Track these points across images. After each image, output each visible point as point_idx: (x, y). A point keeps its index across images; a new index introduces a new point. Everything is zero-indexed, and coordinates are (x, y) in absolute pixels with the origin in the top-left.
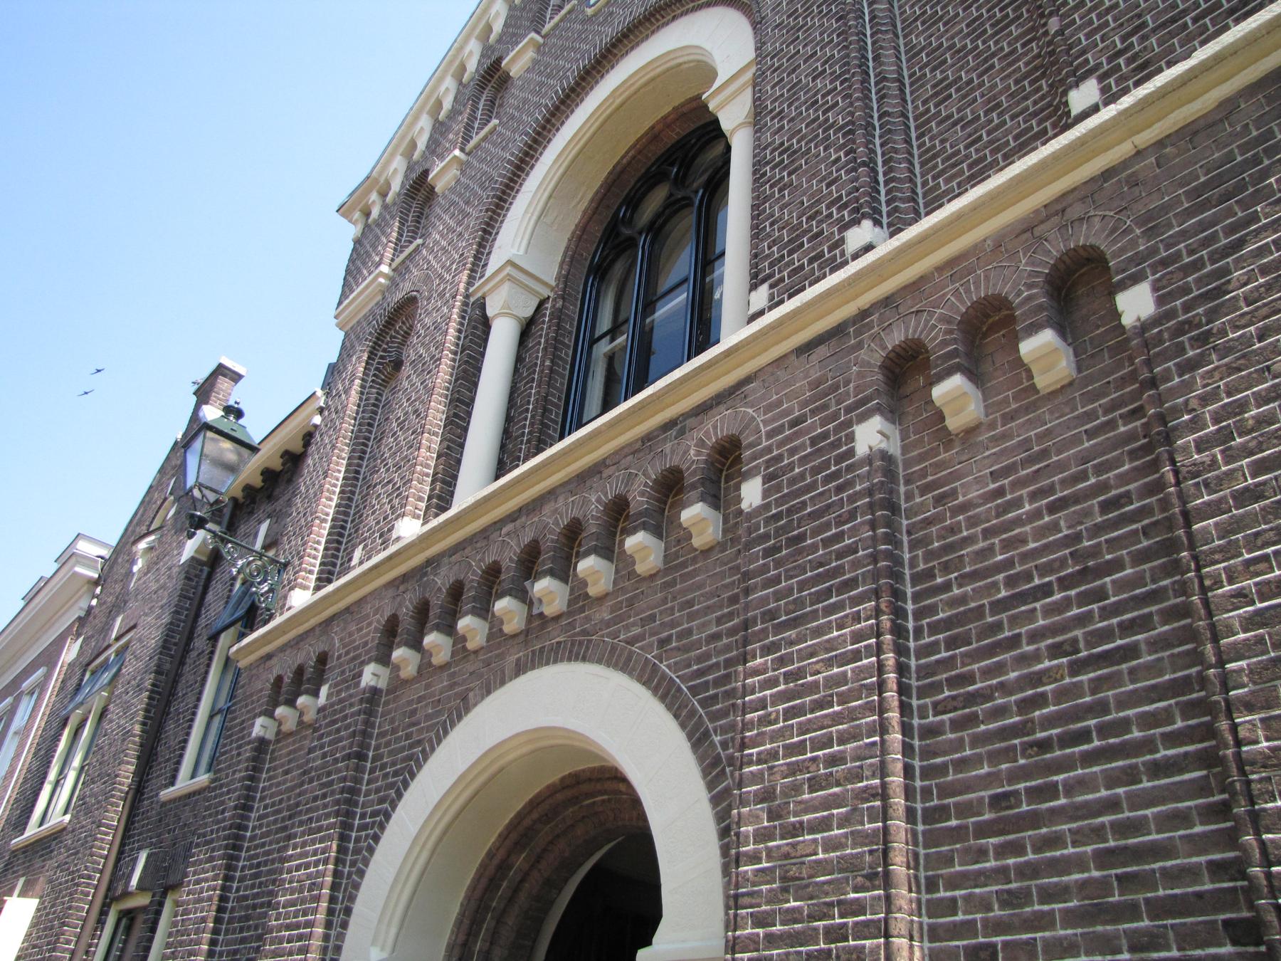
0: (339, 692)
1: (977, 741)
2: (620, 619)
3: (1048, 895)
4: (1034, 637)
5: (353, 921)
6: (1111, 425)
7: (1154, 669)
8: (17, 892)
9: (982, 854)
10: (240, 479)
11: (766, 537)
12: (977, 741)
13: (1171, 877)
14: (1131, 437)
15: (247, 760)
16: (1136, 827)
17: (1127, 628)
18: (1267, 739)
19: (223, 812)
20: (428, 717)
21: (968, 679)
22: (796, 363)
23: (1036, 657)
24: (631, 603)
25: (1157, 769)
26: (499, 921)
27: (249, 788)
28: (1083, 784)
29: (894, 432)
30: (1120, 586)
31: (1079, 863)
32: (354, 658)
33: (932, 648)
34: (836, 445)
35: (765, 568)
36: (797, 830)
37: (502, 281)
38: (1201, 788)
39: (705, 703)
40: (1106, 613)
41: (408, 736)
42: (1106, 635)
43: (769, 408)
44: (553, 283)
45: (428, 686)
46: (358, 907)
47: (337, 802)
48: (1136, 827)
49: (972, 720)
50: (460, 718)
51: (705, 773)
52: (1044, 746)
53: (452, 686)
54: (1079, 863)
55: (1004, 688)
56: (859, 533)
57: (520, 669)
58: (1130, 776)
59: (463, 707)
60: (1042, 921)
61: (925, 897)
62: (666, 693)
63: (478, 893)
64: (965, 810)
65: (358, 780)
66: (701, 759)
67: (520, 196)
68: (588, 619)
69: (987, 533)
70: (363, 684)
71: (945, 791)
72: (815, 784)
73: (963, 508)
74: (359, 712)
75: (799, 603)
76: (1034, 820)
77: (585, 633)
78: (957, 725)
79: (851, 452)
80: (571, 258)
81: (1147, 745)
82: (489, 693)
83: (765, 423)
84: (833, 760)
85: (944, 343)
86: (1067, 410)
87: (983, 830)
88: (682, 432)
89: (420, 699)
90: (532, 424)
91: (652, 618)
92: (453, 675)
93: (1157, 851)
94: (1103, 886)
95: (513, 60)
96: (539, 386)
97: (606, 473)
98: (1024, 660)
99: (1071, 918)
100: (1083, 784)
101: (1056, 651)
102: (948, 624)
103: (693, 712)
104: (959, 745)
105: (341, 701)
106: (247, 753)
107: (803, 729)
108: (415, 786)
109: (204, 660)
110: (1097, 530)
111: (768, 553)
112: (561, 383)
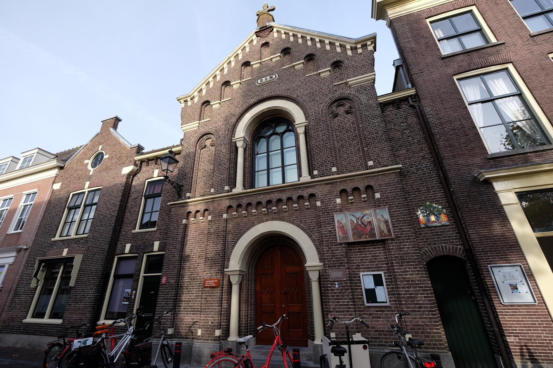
3: (366, 260)
8: (541, 234)
10: (511, 271)
18: (273, 327)
24: (293, 214)
31: (369, 257)
38: (383, 250)
46: (231, 258)
54: (369, 257)
57: (267, 220)
59: (253, 225)
60: (366, 262)
62: (303, 229)
66: (311, 239)
86: (334, 169)
88: (302, 190)
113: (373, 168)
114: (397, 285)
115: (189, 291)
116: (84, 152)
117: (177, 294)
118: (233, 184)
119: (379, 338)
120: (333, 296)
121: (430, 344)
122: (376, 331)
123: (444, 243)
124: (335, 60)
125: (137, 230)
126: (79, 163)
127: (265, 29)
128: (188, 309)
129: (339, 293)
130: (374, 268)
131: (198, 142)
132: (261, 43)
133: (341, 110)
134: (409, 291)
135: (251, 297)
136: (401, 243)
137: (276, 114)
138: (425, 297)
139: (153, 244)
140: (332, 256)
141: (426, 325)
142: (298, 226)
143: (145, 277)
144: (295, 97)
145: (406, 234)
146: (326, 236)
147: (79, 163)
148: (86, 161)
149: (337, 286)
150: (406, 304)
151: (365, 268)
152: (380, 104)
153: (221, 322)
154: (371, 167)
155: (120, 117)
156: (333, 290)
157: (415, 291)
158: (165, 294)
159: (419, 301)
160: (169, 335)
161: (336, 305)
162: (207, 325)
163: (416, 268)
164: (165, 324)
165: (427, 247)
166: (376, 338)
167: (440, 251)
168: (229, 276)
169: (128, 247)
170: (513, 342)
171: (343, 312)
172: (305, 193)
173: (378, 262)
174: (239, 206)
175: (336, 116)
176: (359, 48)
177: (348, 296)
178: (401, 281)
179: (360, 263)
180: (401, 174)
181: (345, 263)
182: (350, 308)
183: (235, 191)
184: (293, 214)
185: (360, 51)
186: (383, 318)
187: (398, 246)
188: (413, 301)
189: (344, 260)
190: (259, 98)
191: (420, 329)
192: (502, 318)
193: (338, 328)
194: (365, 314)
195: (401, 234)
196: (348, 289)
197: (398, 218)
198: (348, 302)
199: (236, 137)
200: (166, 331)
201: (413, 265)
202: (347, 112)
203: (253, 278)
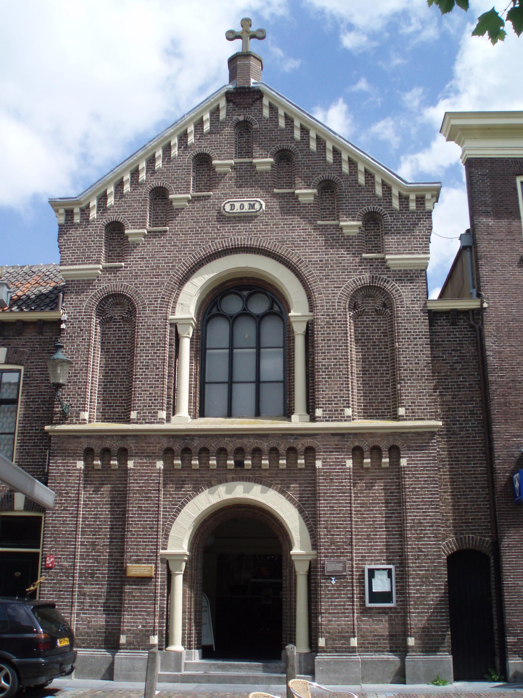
1: (365, 525)
13: (392, 549)
14: (396, 482)
17: (391, 513)
25: (393, 535)
30: (391, 506)
31: (380, 546)
36: (333, 535)
38: (398, 538)
52: (376, 528)
55: (370, 517)
61: (40, 550)
71: (359, 532)
72: (337, 528)
81: (392, 531)
93: (391, 545)
97: (269, 438)
121: (432, 647)
123: (473, 533)
129: (335, 590)
145: (430, 519)
159: (430, 601)
177: (347, 594)
178: (413, 578)
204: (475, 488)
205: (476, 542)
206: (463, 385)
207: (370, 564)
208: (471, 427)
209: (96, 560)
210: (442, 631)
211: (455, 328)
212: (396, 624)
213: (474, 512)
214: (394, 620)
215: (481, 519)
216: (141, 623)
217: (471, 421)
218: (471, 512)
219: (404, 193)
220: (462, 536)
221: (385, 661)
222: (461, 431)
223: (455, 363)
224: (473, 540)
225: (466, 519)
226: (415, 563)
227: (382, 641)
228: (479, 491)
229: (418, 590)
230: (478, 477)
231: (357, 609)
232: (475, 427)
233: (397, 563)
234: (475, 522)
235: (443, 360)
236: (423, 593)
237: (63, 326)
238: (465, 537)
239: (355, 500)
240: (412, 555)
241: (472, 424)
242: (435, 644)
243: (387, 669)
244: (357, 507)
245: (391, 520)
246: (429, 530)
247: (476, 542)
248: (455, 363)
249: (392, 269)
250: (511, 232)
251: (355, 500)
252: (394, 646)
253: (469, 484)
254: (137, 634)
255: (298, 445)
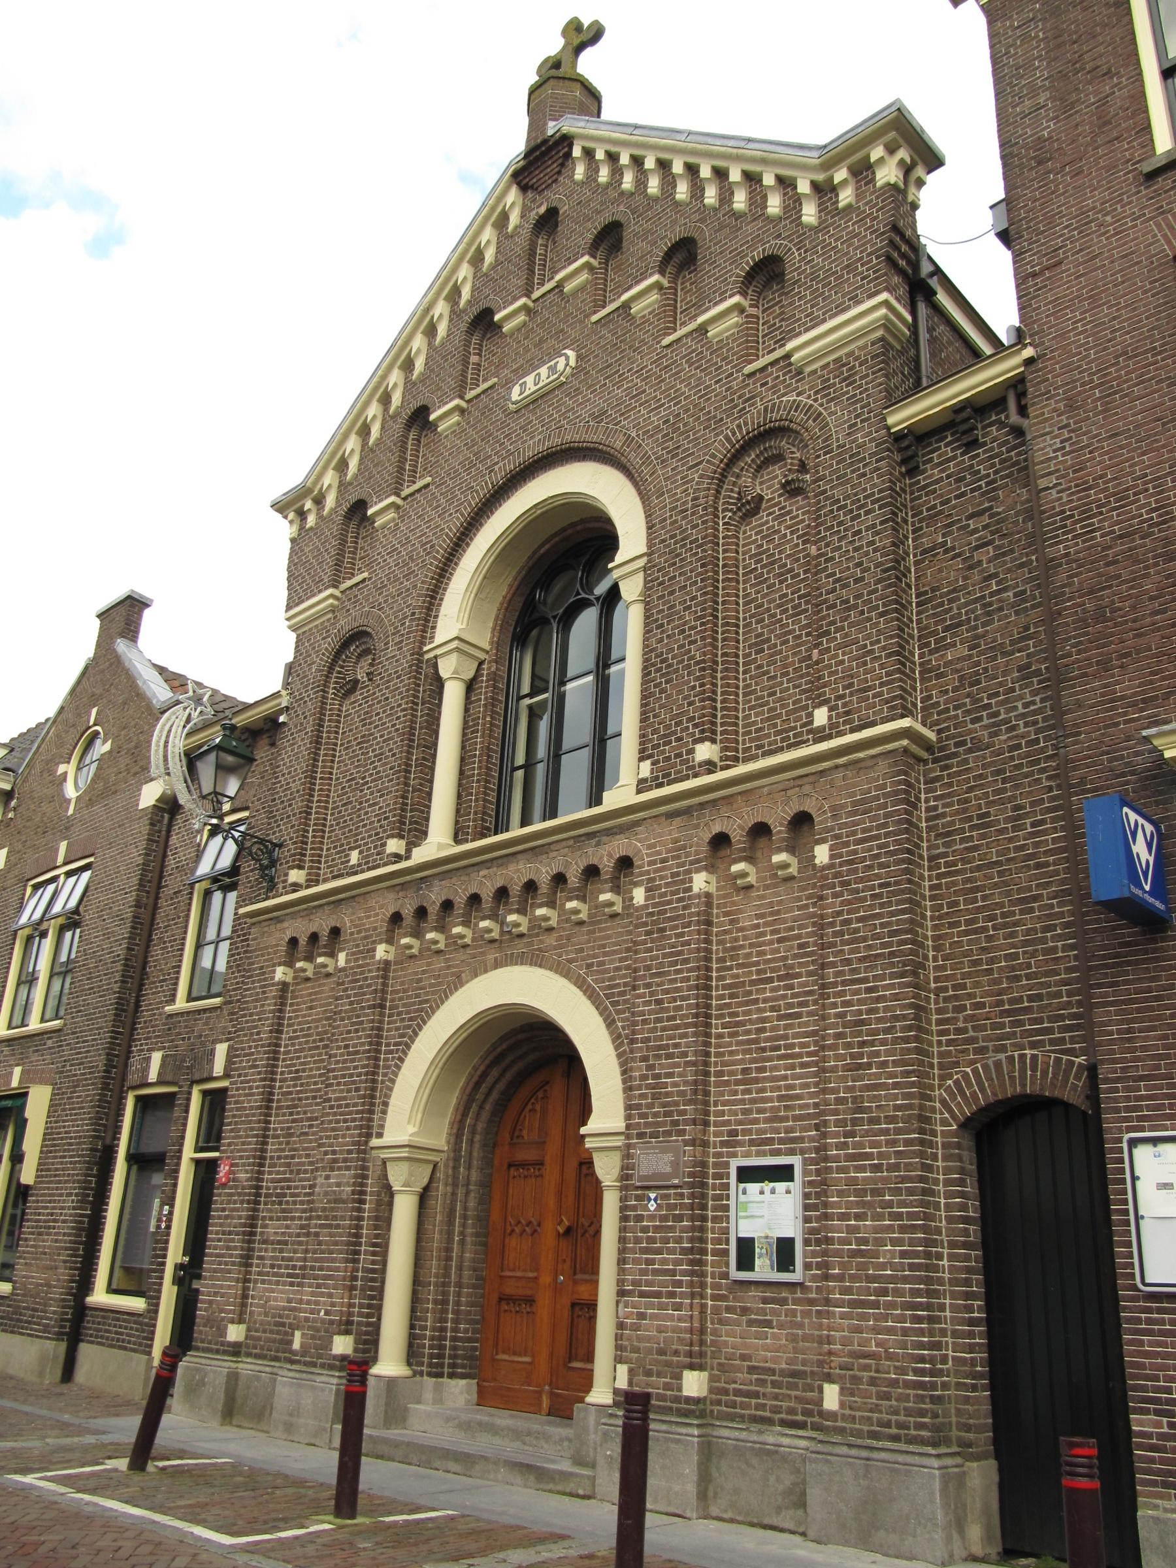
0: (356, 960)
1: (739, 1043)
2: (561, 947)
3: (759, 1111)
4: (765, 1000)
5: (390, 1109)
6: (806, 906)
7: (806, 1024)
9: (735, 1093)
11: (645, 924)
12: (739, 1043)
13: (801, 1107)
15: (274, 997)
16: (792, 1087)
19: (258, 1033)
20: (432, 985)
21: (736, 1014)
22: (642, 1167)
23: (764, 1010)
24: (568, 938)
26: (481, 1107)
27: (279, 1018)
28: (775, 1068)
29: (713, 879)
30: (801, 985)
31: (770, 1099)
32: (366, 938)
33: (722, 997)
34: (683, 882)
35: (645, 942)
37: (451, 651)
39: (614, 1004)
40: (794, 996)
41: (417, 996)
42: (790, 1006)
43: (649, 847)
44: (487, 647)
45: (429, 964)
46: (393, 1101)
47: (370, 1036)
48: (792, 1087)
49: (736, 1034)
50: (456, 989)
51: (614, 1041)
52: (764, 1050)
53: (448, 967)
54: (770, 1099)
55: (751, 1021)
56: (692, 933)
57: (497, 965)
58: (793, 1067)
59: (458, 983)
62: (592, 995)
63: (468, 1091)
64: (731, 1073)
65: (381, 1022)
66: (611, 1034)
67: (459, 570)
68: (542, 942)
69: (751, 945)
70: (378, 958)
71: (724, 1064)
73: (742, 929)
74: (377, 977)
75: (661, 965)
76: (757, 1080)
77: (540, 950)
78: (731, 1035)
79: (690, 889)
80: (501, 627)
81: (800, 1055)
82: (476, 976)
83: (648, 855)
84: (676, 1046)
85: (739, 842)
87: (737, 1083)
88: (598, 844)
89: (424, 972)
90: (480, 768)
91: (582, 950)
92: (447, 960)
94: (778, 1109)
95: (441, 418)
96: (483, 736)
98: (760, 1010)
99: (766, 1121)
100: (775, 1068)
101: (772, 1009)
102: (730, 986)
103: (606, 1008)
104: (730, 1044)
105: (359, 966)
106: (273, 992)
107: (664, 1029)
108: (427, 1029)
109: (183, 897)
110: (796, 956)
111: (648, 933)
112: (498, 733)
113: (830, 737)
114: (826, 1205)
115: (284, 1211)
116: (58, 736)
117: (254, 1218)
118: (417, 832)
119: (756, 1395)
120: (637, 1240)
121: (888, 1425)
122: (752, 1370)
123: (1033, 1045)
124: (757, 254)
125: (181, 1004)
126: (45, 775)
127: (543, 154)
128: (280, 1267)
129: (657, 1229)
130: (781, 1141)
131: (331, 669)
132: (533, 216)
133: (768, 485)
134: (856, 1229)
135: (462, 1242)
136: (863, 1044)
137: (582, 521)
138: (903, 1254)
139: (212, 1052)
140: (654, 1096)
141: (890, 1357)
142: (580, 984)
143: (198, 1162)
144: (618, 445)
145: (886, 1009)
146: (645, 1022)
147: (45, 775)
148: (62, 768)
149: (652, 1206)
150: (841, 1278)
151: (752, 1143)
152: (898, 437)
153: (350, 1314)
154: (710, 766)
155: (144, 590)
156: (639, 1218)
157: (876, 1230)
158: (227, 1217)
159: (883, 1267)
160: (230, 1344)
161: (644, 1272)
162: (314, 1320)
163: (894, 1143)
164: (222, 1311)
165: (972, 1063)
166: (748, 1394)
167: (1012, 1078)
168: (384, 1162)
169: (156, 1058)
170: (1149, 1435)
171: (658, 1295)
172: (605, 856)
173: (796, 1118)
174: (421, 912)
175: (750, 508)
176: (844, 182)
177: (679, 1240)
178: (840, 1193)
179: (740, 1123)
180: (916, 757)
181: (686, 1122)
182: (679, 1284)
183: (420, 855)
184: (568, 938)
185: (846, 196)
186: (781, 1326)
187: (853, 1056)
188: (862, 1267)
189: (684, 1112)
190: (510, 466)
191: (866, 1368)
192: (1131, 1342)
193: (636, 1350)
194: (729, 1309)
195: (869, 1012)
196: (679, 1218)
197: (870, 947)
198: (677, 1262)
199: (440, 638)
200: (222, 1332)
201: (886, 1132)
202: (792, 490)
203: (475, 1175)
204: (1035, 898)
205: (1045, 1073)
206: (1000, 600)
207: (747, 1155)
208: (1023, 716)
209: (288, 1165)
210: (917, 1372)
211: (978, 455)
212: (806, 1338)
213: (1035, 976)
214: (801, 1326)
215: (1058, 994)
216: (324, 1304)
217: (1021, 697)
218: (1028, 977)
219: (820, 177)
220: (1002, 1056)
221: (769, 1453)
222: (996, 734)
223: (977, 548)
224: (1034, 1069)
225: (1012, 1001)
226: (844, 1146)
227: (769, 1390)
228: (1052, 906)
229: (851, 1230)
230: (1047, 864)
231: (472, 1235)
232: (1034, 713)
233: (809, 1150)
234: (1041, 1009)
235: (946, 551)
236: (865, 1241)
237: (282, 719)
238: (1011, 1059)
239: (719, 979)
240: (837, 1123)
241: (1026, 705)
242: (896, 1413)
243: (772, 1479)
244: (722, 997)
245: (800, 1025)
246: (883, 1043)
247: (1045, 1073)
248: (977, 548)
249: (808, 369)
250: (1109, 122)
251: (719, 979)
252: (799, 1407)
253: (1019, 891)
254: (317, 1330)
255: (601, 858)
